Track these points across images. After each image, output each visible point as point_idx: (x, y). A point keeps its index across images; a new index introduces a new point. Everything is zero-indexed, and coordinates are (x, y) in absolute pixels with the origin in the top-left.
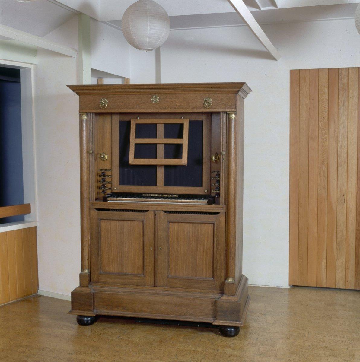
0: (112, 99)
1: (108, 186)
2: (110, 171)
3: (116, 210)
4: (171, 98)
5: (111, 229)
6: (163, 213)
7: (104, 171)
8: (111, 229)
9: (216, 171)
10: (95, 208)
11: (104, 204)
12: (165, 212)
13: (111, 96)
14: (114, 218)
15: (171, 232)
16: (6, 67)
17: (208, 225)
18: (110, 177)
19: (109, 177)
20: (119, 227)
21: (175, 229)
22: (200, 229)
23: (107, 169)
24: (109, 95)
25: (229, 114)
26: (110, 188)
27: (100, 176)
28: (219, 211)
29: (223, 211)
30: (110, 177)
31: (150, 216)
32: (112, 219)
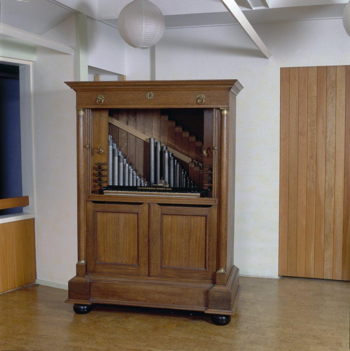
6: (157, 206)
7: (100, 164)
12: (160, 204)
18: (106, 171)
19: (105, 170)
20: (114, 219)
21: (168, 221)
24: (105, 91)
26: (106, 181)
28: (211, 204)
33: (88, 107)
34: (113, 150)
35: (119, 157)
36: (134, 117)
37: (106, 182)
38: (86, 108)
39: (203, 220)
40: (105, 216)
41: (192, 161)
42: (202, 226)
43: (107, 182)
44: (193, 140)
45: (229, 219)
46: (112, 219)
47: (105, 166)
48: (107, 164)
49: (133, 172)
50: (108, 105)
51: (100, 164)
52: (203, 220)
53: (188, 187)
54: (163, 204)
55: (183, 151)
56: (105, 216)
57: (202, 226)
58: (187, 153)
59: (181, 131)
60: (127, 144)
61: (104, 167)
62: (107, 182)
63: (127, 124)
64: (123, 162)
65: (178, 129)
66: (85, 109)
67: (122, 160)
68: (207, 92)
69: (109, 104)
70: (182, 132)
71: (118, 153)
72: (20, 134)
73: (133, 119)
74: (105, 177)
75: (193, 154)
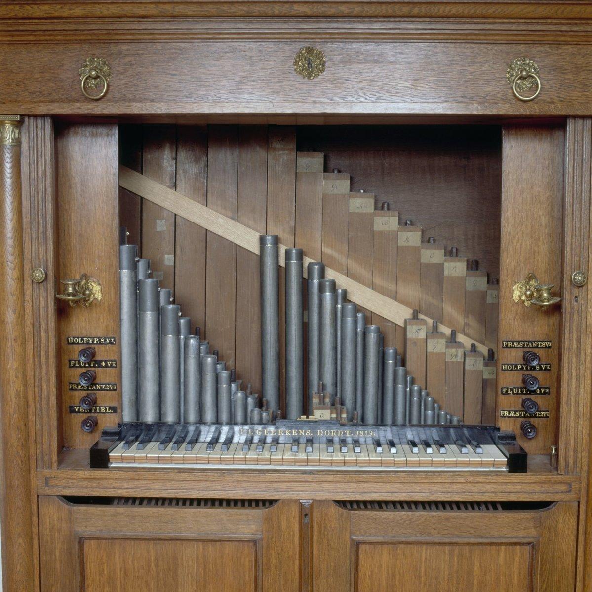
0: (127, 59)
1: (105, 399)
2: (110, 343)
3: (137, 502)
4: (138, 54)
5: (125, 573)
6: (335, 510)
7: (88, 343)
8: (125, 573)
9: (519, 342)
10: (58, 496)
11: (99, 479)
12: (342, 504)
13: (125, 48)
14: (139, 533)
15: (367, 580)
16: (99, 505)
17: (511, 548)
18: (111, 366)
19: (106, 366)
20: (157, 566)
21: (380, 566)
22: (477, 563)
23: (100, 335)
24: (118, 42)
25: (90, 77)
26: (110, 408)
27: (72, 363)
28: (556, 498)
29: (566, 497)
30: (111, 366)
31: (284, 525)
32: (129, 534)
33: (44, 109)
34: (137, 285)
35: (159, 312)
36: (197, 161)
37: (114, 409)
38: (29, 116)
39: (517, 559)
40: (117, 555)
41: (415, 316)
42: (515, 582)
43: (115, 412)
44: (410, 244)
45: (302, 379)
46: (149, 566)
47: (107, 347)
48: (116, 342)
49: (215, 369)
50: (130, 100)
51: (88, 343)
52: (517, 559)
53: (448, 424)
54: (358, 502)
55: (378, 281)
56: (117, 555)
57: (515, 582)
58: (392, 286)
59: (370, 209)
60: (172, 256)
61: (102, 354)
62: (115, 412)
63: (175, 187)
64: (177, 333)
65: (357, 205)
66: (26, 119)
67: (170, 325)
68: (548, 49)
69: (131, 96)
70: (373, 215)
71: (157, 296)
72: (343, 125)
73: (573, 121)
74: (110, 390)
75: (412, 291)
